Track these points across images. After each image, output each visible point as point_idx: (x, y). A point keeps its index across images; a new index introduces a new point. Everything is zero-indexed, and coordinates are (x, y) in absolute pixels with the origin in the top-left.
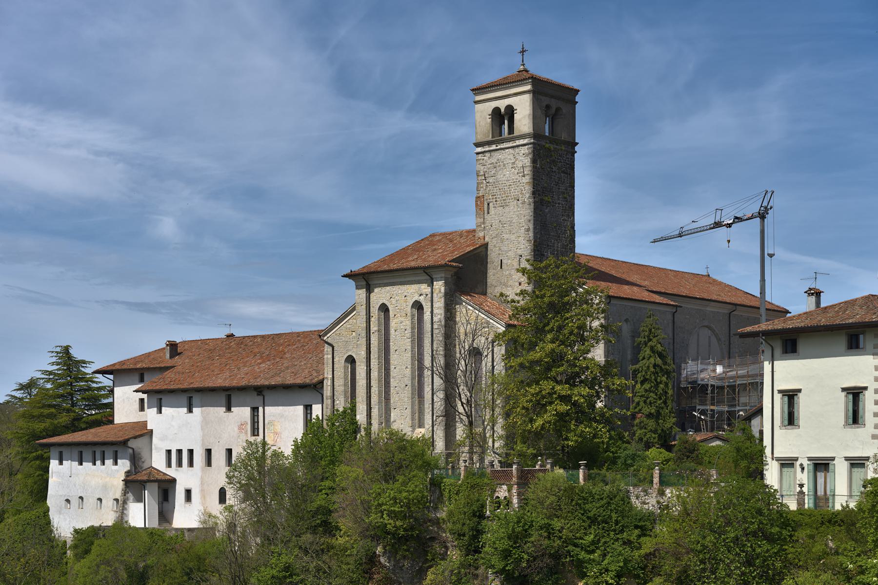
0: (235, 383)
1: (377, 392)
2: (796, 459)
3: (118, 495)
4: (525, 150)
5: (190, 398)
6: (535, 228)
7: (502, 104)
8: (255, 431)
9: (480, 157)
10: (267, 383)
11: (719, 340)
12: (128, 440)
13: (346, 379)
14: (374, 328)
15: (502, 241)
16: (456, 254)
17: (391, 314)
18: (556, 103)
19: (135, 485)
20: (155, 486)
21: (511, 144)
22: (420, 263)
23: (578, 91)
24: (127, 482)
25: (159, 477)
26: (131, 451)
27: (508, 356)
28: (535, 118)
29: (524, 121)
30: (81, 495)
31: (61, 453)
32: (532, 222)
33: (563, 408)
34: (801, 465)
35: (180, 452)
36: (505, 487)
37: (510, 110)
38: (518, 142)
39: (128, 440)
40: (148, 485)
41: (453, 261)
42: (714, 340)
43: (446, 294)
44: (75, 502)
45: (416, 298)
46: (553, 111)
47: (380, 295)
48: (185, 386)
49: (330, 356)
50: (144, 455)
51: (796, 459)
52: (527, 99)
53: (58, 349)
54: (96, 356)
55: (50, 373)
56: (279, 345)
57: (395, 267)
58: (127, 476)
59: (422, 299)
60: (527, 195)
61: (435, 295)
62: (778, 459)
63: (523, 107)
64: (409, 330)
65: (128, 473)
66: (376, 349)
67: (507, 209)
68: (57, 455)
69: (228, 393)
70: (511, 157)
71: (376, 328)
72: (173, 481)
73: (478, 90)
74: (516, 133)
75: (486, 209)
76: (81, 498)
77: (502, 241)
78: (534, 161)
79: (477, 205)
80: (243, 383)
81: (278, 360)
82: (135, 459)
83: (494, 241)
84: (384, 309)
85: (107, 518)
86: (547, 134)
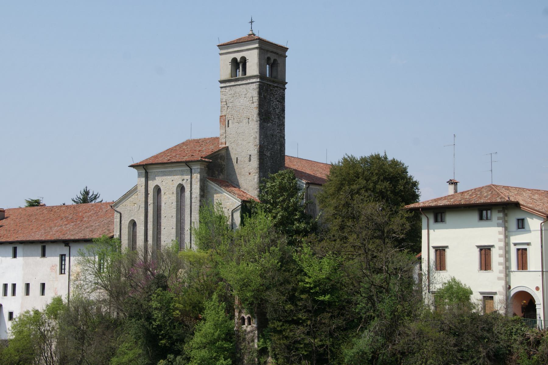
4: (255, 86)
7: (238, 56)
9: (223, 89)
10: (72, 238)
21: (244, 82)
29: (253, 68)
32: (258, 133)
37: (244, 61)
38: (249, 81)
41: (205, 158)
46: (272, 61)
49: (118, 220)
52: (256, 52)
70: (245, 90)
74: (248, 74)
78: (260, 93)
79: (220, 121)
84: (158, 190)
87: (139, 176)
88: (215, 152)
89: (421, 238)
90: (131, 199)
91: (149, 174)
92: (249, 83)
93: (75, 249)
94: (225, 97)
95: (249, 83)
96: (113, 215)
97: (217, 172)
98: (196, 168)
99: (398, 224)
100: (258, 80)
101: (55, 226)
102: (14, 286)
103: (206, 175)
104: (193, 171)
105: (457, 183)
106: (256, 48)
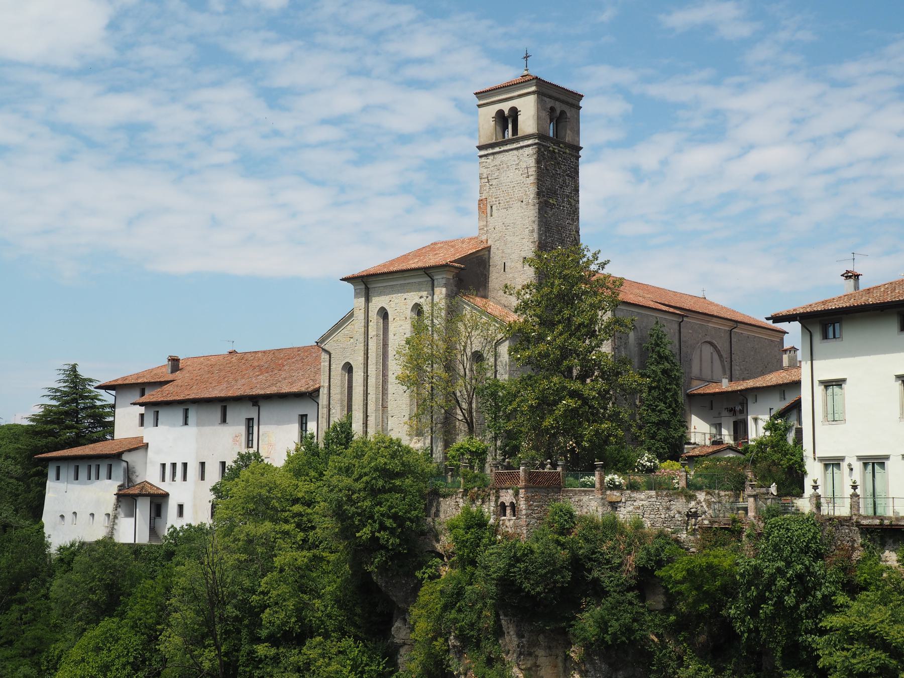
1: (374, 400)
2: (842, 459)
3: (110, 510)
4: (530, 151)
5: (186, 411)
6: (539, 229)
7: (506, 107)
8: (249, 443)
9: (483, 159)
10: (262, 392)
11: (720, 356)
12: (122, 453)
13: (342, 387)
14: (372, 332)
16: (458, 256)
17: (390, 318)
18: (561, 106)
19: (127, 499)
21: (515, 146)
22: (421, 265)
24: (120, 497)
26: (125, 464)
27: (513, 350)
29: (528, 122)
30: (77, 511)
32: (536, 222)
33: (571, 403)
34: (850, 465)
35: (174, 465)
36: (511, 492)
37: (514, 112)
38: (522, 144)
39: (122, 453)
41: (455, 261)
42: (716, 356)
44: (69, 517)
47: (378, 302)
48: (181, 397)
49: (327, 364)
50: (139, 469)
51: (842, 459)
52: (532, 99)
53: (66, 367)
54: (98, 371)
55: (57, 390)
56: (279, 359)
57: (395, 269)
58: (119, 490)
60: (532, 196)
62: (821, 459)
63: (528, 111)
65: (121, 487)
66: (374, 355)
67: (510, 211)
70: (515, 158)
71: (375, 333)
72: (166, 496)
74: (520, 134)
76: (75, 513)
78: (538, 162)
79: (479, 207)
80: (238, 393)
81: (276, 372)
82: (129, 473)
83: (497, 244)
84: (384, 314)
85: (94, 533)
86: (551, 135)
87: (357, 295)
90: (345, 331)
91: (371, 290)
92: (522, 147)
93: (267, 411)
94: (485, 170)
95: (522, 147)
96: (319, 356)
98: (440, 278)
101: (243, 378)
102: (185, 465)
104: (436, 283)
105: (858, 276)
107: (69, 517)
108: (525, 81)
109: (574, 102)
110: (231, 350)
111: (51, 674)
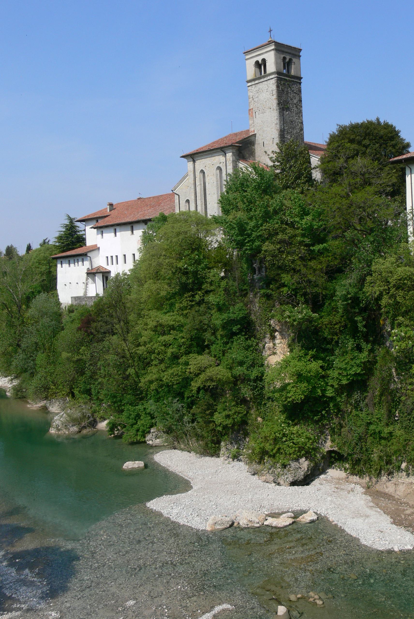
0: (134, 220)
3: (84, 281)
4: (273, 81)
7: (260, 59)
9: (250, 88)
15: (264, 131)
18: (289, 55)
20: (101, 275)
21: (265, 79)
23: (301, 50)
25: (102, 270)
28: (277, 63)
29: (271, 67)
31: (61, 262)
32: (278, 119)
37: (264, 60)
38: (269, 78)
40: (97, 275)
41: (236, 143)
43: (233, 161)
45: (218, 165)
46: (287, 60)
49: (178, 201)
52: (273, 53)
59: (221, 165)
60: (275, 105)
61: (227, 162)
63: (271, 59)
64: (215, 183)
68: (60, 262)
69: (131, 225)
70: (266, 86)
71: (199, 183)
73: (246, 53)
74: (268, 71)
75: (254, 117)
76: (70, 283)
77: (264, 131)
78: (278, 87)
84: (202, 172)
88: (246, 138)
89: (405, 188)
92: (269, 80)
95: (269, 80)
97: (247, 155)
99: (387, 178)
100: (276, 76)
103: (237, 157)
106: (273, 49)
107: (68, 284)
108: (270, 43)
109: (297, 53)
110: (138, 197)
111: (8, 356)
